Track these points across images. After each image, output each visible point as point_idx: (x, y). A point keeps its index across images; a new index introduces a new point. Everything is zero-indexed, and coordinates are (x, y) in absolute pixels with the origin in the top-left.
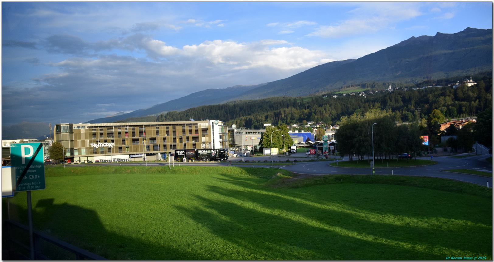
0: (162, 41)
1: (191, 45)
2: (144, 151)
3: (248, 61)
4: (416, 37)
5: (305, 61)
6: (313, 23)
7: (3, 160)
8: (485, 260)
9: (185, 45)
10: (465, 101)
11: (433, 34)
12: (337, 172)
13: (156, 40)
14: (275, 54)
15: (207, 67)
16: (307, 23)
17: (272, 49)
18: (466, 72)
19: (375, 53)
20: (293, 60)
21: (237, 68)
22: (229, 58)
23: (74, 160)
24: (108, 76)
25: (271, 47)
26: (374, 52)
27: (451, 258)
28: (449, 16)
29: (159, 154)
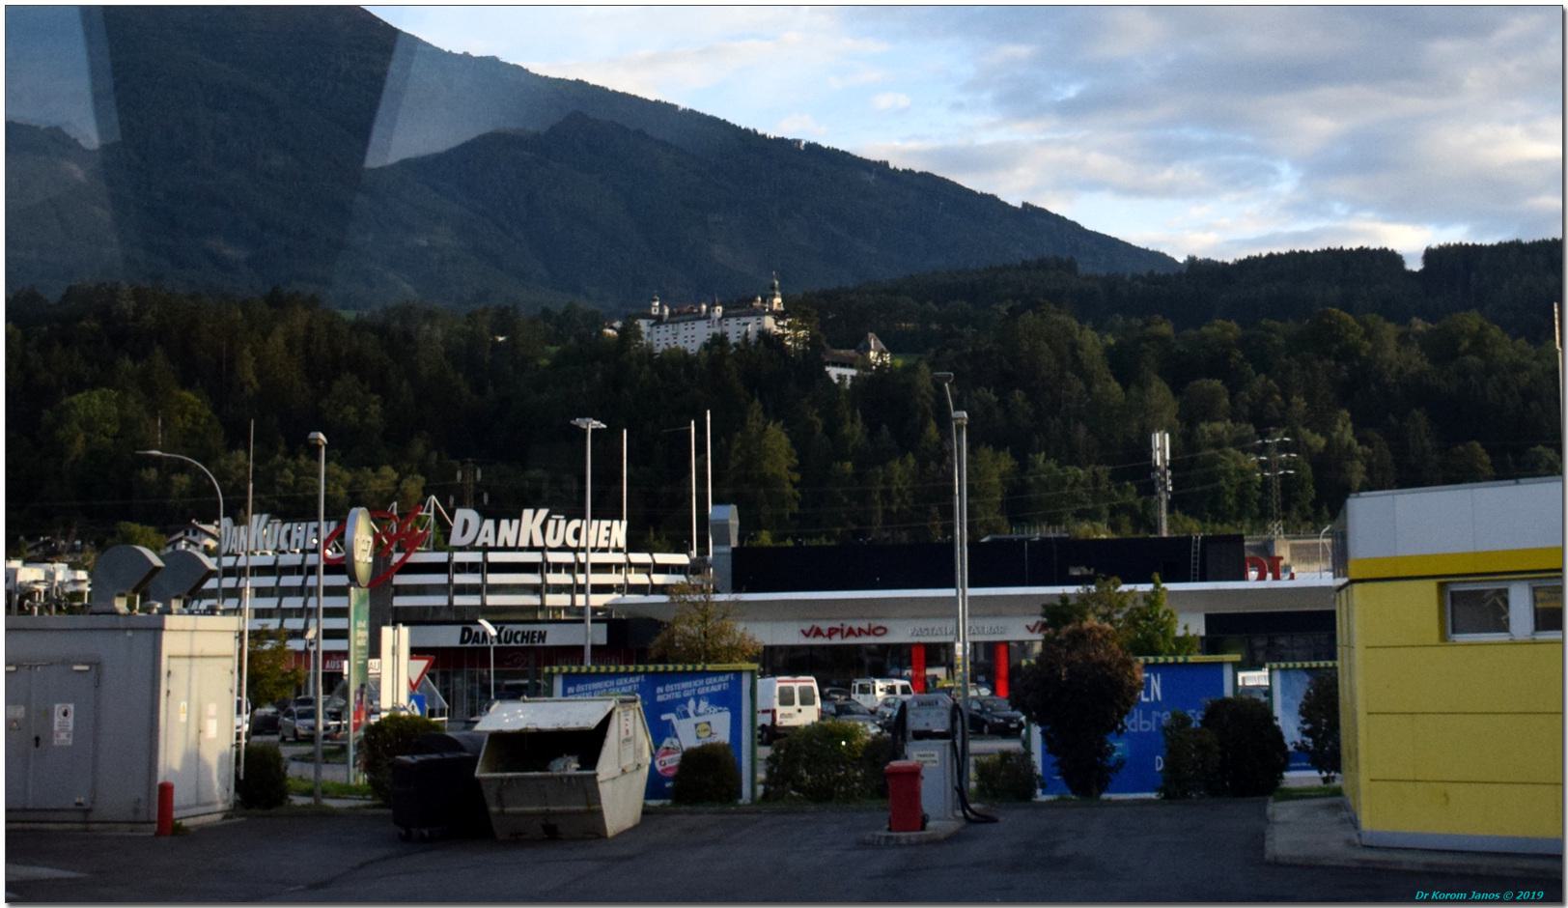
7: (1561, 578)
8: (1537, 901)
12: (194, 521)
19: (614, 92)
27: (1431, 894)
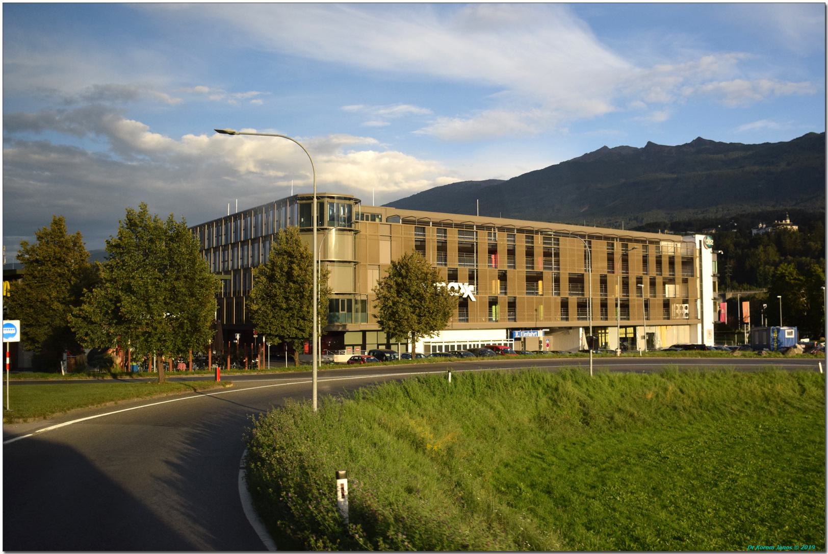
0: (144, 123)
1: (197, 134)
2: (621, 319)
3: (303, 172)
4: (610, 147)
5: (408, 179)
6: (425, 111)
9: (186, 134)
10: (806, 256)
11: (641, 144)
13: (131, 120)
14: (354, 162)
15: (226, 178)
16: (414, 109)
17: (350, 153)
18: (702, 213)
20: (386, 176)
21: (283, 183)
22: (268, 165)
23: (346, 343)
24: (31, 182)
25: (347, 149)
26: (539, 169)
28: (660, 117)
29: (581, 329)
